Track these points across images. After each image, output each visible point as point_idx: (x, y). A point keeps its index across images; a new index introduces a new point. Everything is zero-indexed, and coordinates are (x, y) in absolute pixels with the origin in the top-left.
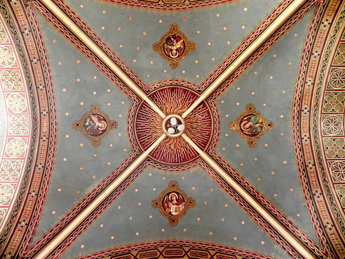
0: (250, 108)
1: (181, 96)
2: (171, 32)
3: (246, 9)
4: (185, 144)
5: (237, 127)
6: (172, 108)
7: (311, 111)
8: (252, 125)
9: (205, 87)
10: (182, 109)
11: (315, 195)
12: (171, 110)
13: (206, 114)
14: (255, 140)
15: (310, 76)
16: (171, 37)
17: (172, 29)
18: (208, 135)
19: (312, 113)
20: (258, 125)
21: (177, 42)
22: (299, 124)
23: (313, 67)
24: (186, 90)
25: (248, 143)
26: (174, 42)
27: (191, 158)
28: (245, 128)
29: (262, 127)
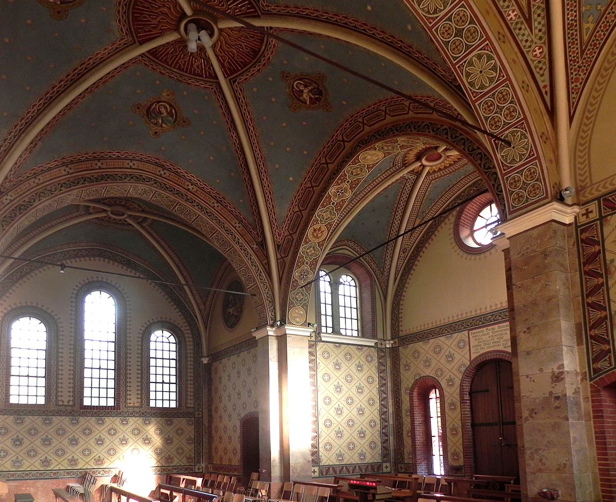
0: (184, 122)
1: (239, 56)
2: (325, 102)
3: (291, 179)
4: (163, 29)
5: (166, 98)
6: (229, 36)
7: (160, 178)
8: (162, 116)
9: (236, 91)
10: (221, 47)
11: (67, 167)
12: (227, 34)
13: (198, 71)
14: (141, 112)
15: (197, 190)
16: (321, 97)
17: (327, 104)
18: (165, 60)
19: (157, 178)
20: (160, 122)
21: (311, 98)
22: (148, 162)
23: (205, 197)
24: (245, 66)
25: (139, 104)
26: (312, 95)
27: (136, 30)
28: (160, 107)
29: (156, 124)
